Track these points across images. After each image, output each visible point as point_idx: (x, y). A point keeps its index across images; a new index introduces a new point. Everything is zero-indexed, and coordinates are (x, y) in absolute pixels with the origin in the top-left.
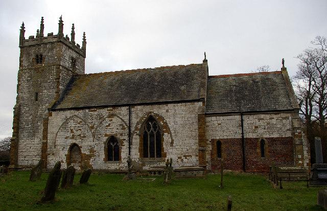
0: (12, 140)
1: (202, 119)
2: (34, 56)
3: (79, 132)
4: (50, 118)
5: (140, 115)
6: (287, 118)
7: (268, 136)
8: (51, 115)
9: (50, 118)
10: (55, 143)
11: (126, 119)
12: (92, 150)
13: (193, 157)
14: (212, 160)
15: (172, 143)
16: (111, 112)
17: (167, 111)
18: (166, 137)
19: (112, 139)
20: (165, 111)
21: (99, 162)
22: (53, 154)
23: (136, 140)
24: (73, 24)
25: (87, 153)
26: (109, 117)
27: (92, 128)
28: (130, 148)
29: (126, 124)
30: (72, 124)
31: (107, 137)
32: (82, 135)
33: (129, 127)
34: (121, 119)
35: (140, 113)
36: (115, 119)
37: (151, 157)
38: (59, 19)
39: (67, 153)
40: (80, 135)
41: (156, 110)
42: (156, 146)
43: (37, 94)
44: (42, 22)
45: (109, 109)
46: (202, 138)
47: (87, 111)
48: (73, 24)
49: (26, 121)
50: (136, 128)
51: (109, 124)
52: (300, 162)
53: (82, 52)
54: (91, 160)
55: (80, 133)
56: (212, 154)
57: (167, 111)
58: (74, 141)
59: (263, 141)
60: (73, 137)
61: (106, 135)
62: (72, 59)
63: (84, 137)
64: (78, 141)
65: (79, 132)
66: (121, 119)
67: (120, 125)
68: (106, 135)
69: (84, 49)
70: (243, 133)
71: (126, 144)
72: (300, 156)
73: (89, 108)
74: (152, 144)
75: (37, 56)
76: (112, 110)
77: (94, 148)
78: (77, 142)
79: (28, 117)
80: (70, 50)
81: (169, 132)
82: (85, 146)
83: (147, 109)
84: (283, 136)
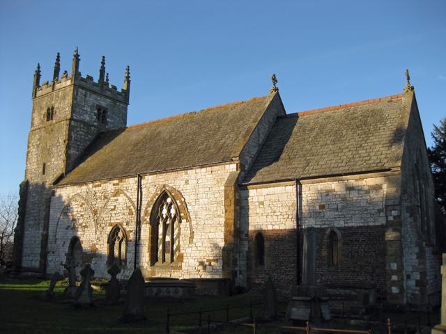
1: (240, 187)
7: (342, 224)
10: (55, 236)
14: (249, 267)
15: (192, 237)
16: (117, 187)
17: (187, 182)
20: (183, 182)
22: (53, 253)
24: (59, 54)
29: (133, 205)
31: (111, 228)
32: (84, 224)
33: (139, 211)
36: (121, 198)
38: (75, 53)
39: (67, 250)
44: (58, 60)
48: (59, 54)
51: (115, 206)
52: (394, 278)
53: (123, 98)
54: (93, 262)
56: (248, 259)
57: (187, 182)
59: (333, 233)
62: (99, 108)
69: (126, 93)
72: (394, 266)
75: (48, 110)
76: (118, 184)
80: (93, 96)
84: (371, 224)
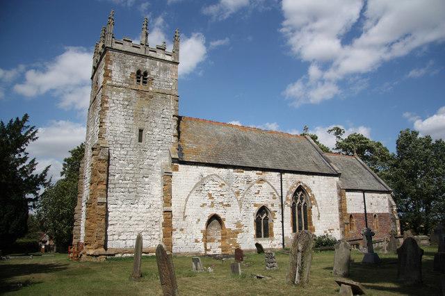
0: (300, 60)
2: (134, 70)
3: (220, 199)
4: (174, 173)
5: (291, 184)
6: (385, 198)
8: (176, 169)
9: (174, 173)
11: (278, 187)
12: (239, 225)
13: (336, 230)
16: (261, 177)
18: (314, 210)
19: (263, 210)
21: (247, 241)
22: (182, 230)
23: (288, 211)
25: (234, 228)
26: (258, 183)
27: (238, 193)
28: (282, 222)
30: (211, 187)
34: (272, 187)
35: (290, 180)
36: (265, 185)
37: (264, 237)
40: (222, 203)
41: (307, 180)
42: (261, 229)
43: (141, 131)
45: (258, 172)
46: (342, 209)
47: (231, 170)
49: (120, 172)
50: (287, 199)
55: (223, 200)
58: (214, 211)
60: (212, 205)
61: (255, 205)
63: (228, 205)
64: (221, 211)
65: (220, 199)
66: (272, 187)
67: (272, 193)
68: (255, 205)
70: (365, 208)
71: (278, 215)
73: (234, 167)
74: (300, 217)
75: (139, 72)
77: (240, 218)
78: (220, 212)
79: (123, 165)
81: (315, 204)
82: (230, 217)
83: (298, 177)
